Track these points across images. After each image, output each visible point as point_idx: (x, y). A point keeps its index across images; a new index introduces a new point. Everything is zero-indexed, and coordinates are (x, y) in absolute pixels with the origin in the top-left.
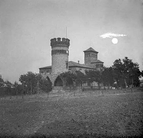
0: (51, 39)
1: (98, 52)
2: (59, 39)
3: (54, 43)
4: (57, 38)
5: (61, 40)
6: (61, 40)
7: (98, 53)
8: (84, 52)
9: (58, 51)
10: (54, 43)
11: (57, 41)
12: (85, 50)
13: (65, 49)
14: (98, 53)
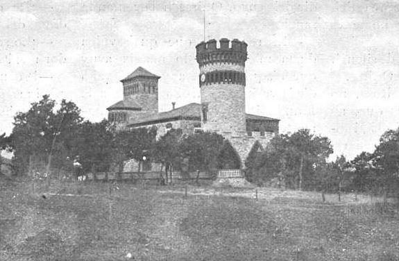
0: (196, 44)
1: (158, 75)
2: (224, 42)
3: (206, 52)
4: (220, 39)
5: (218, 46)
6: (218, 46)
7: (159, 78)
8: (122, 81)
9: (228, 74)
10: (206, 52)
11: (230, 47)
12: (123, 78)
13: (234, 67)
14: (159, 78)
